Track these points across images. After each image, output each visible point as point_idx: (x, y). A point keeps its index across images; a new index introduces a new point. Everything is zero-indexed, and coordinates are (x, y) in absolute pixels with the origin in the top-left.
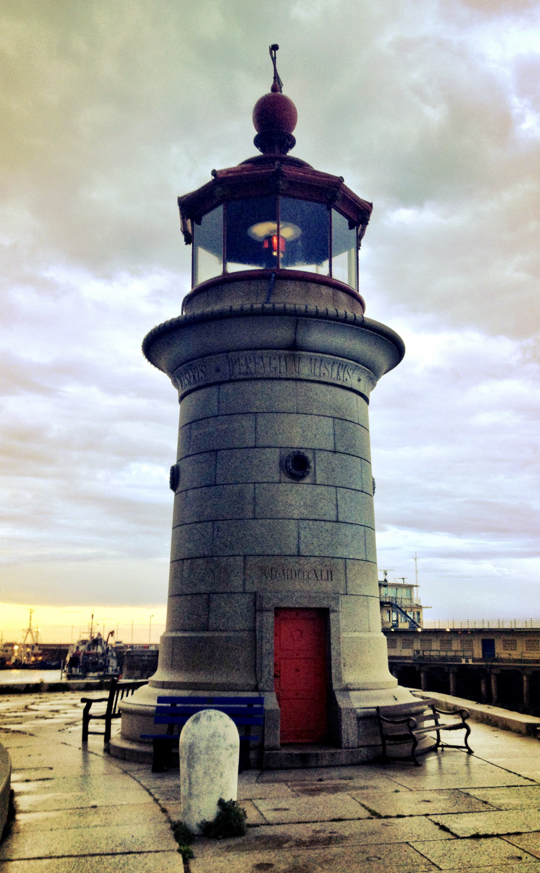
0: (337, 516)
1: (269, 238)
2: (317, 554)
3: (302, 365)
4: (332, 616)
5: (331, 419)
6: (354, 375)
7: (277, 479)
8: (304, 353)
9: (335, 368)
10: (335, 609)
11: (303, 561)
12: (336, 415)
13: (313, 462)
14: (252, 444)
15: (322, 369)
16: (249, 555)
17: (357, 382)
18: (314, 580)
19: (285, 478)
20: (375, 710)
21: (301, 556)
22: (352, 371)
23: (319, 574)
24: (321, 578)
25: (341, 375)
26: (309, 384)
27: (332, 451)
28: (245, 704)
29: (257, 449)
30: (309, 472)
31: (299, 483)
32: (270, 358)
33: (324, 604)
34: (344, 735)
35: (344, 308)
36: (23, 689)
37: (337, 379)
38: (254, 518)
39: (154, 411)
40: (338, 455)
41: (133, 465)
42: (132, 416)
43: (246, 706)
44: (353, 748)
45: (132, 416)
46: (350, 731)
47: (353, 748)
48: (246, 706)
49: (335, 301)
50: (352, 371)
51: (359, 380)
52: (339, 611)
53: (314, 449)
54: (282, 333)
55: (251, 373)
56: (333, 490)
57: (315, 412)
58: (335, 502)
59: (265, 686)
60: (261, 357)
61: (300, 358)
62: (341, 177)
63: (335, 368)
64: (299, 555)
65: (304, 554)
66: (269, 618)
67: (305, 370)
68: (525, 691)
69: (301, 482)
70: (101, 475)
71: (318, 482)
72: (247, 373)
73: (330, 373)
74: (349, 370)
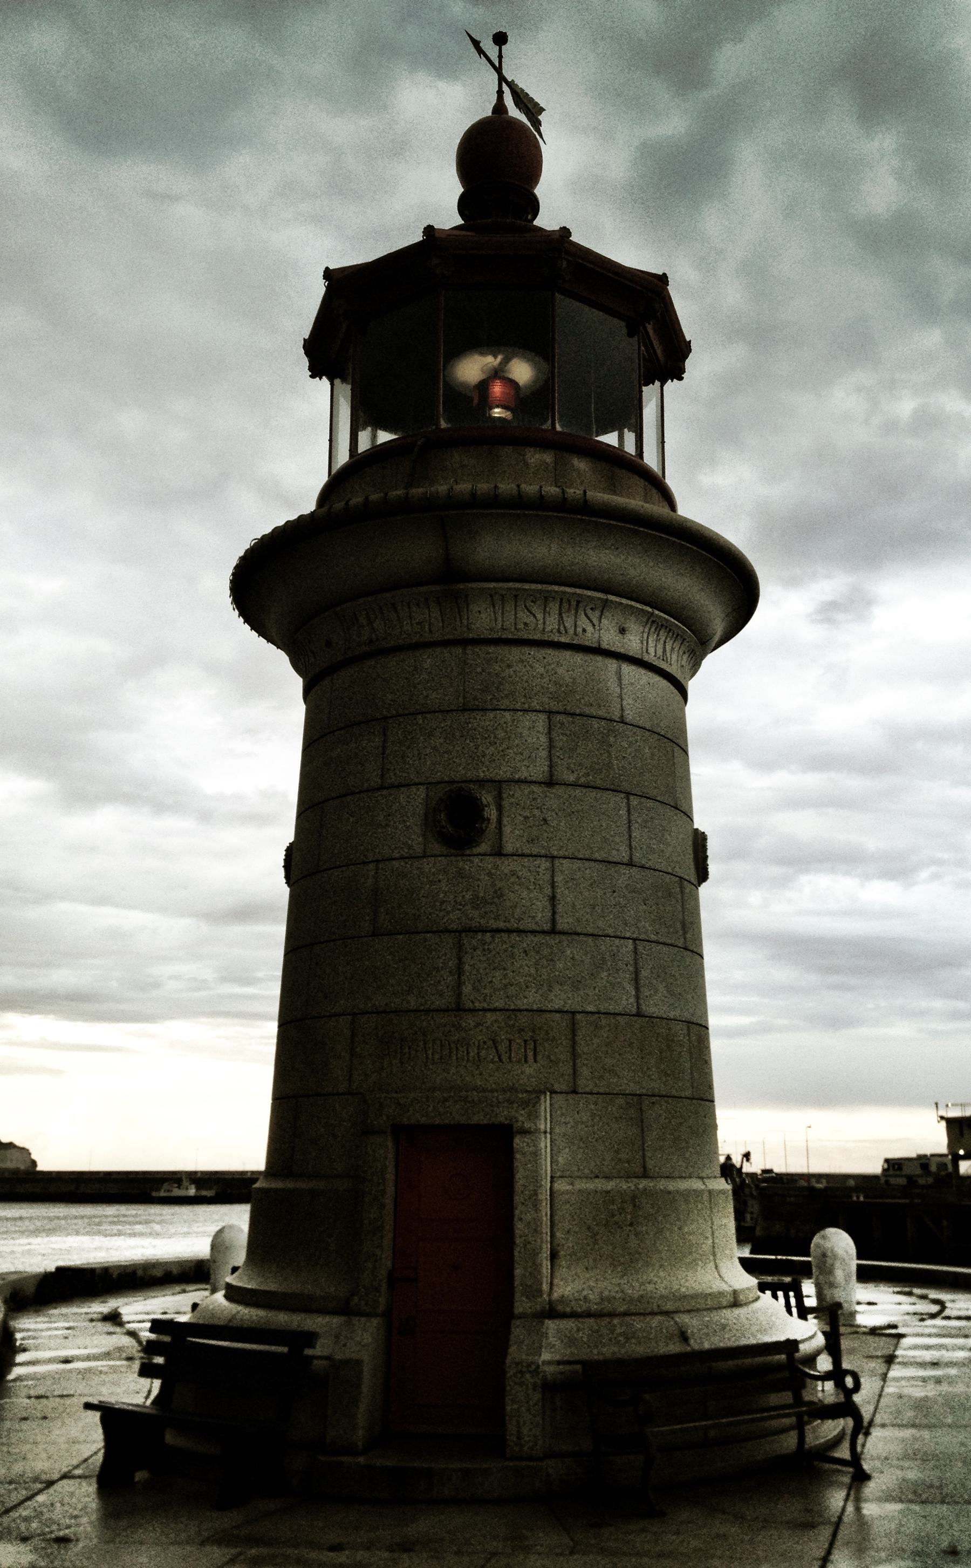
0: (554, 921)
1: (483, 386)
2: (498, 1004)
3: (474, 608)
4: (518, 1141)
5: (543, 717)
6: (605, 621)
7: (419, 849)
8: (474, 585)
9: (554, 607)
10: (527, 1125)
11: (470, 1021)
12: (554, 706)
13: (493, 807)
14: (376, 780)
15: (520, 614)
16: (579, 1012)
17: (619, 637)
18: (492, 1062)
19: (436, 848)
20: (579, 1367)
21: (465, 1010)
22: (597, 613)
23: (502, 1048)
24: (510, 1058)
25: (569, 623)
26: (491, 649)
27: (544, 783)
28: (284, 1345)
29: (385, 792)
30: (482, 831)
31: (463, 855)
32: (409, 604)
33: (502, 1116)
34: (512, 1428)
35: (635, 501)
36: (30, 1289)
37: (559, 631)
38: (374, 935)
39: (238, 741)
40: (560, 790)
41: (804, 879)
42: (795, 802)
43: (285, 1349)
44: (530, 1459)
45: (795, 802)
46: (526, 1420)
47: (530, 1459)
48: (285, 1349)
49: (559, 474)
50: (597, 613)
51: (622, 631)
52: (537, 1131)
53: (500, 782)
54: (417, 551)
55: (377, 640)
56: (545, 864)
57: (505, 703)
58: (548, 891)
59: (363, 1303)
60: (393, 605)
61: (466, 596)
62: (564, 228)
63: (554, 607)
64: (459, 1008)
65: (469, 1005)
66: (383, 1153)
67: (482, 618)
68: (770, 1358)
69: (468, 852)
70: (755, 897)
71: (509, 847)
72: (371, 641)
73: (547, 622)
74: (589, 612)
